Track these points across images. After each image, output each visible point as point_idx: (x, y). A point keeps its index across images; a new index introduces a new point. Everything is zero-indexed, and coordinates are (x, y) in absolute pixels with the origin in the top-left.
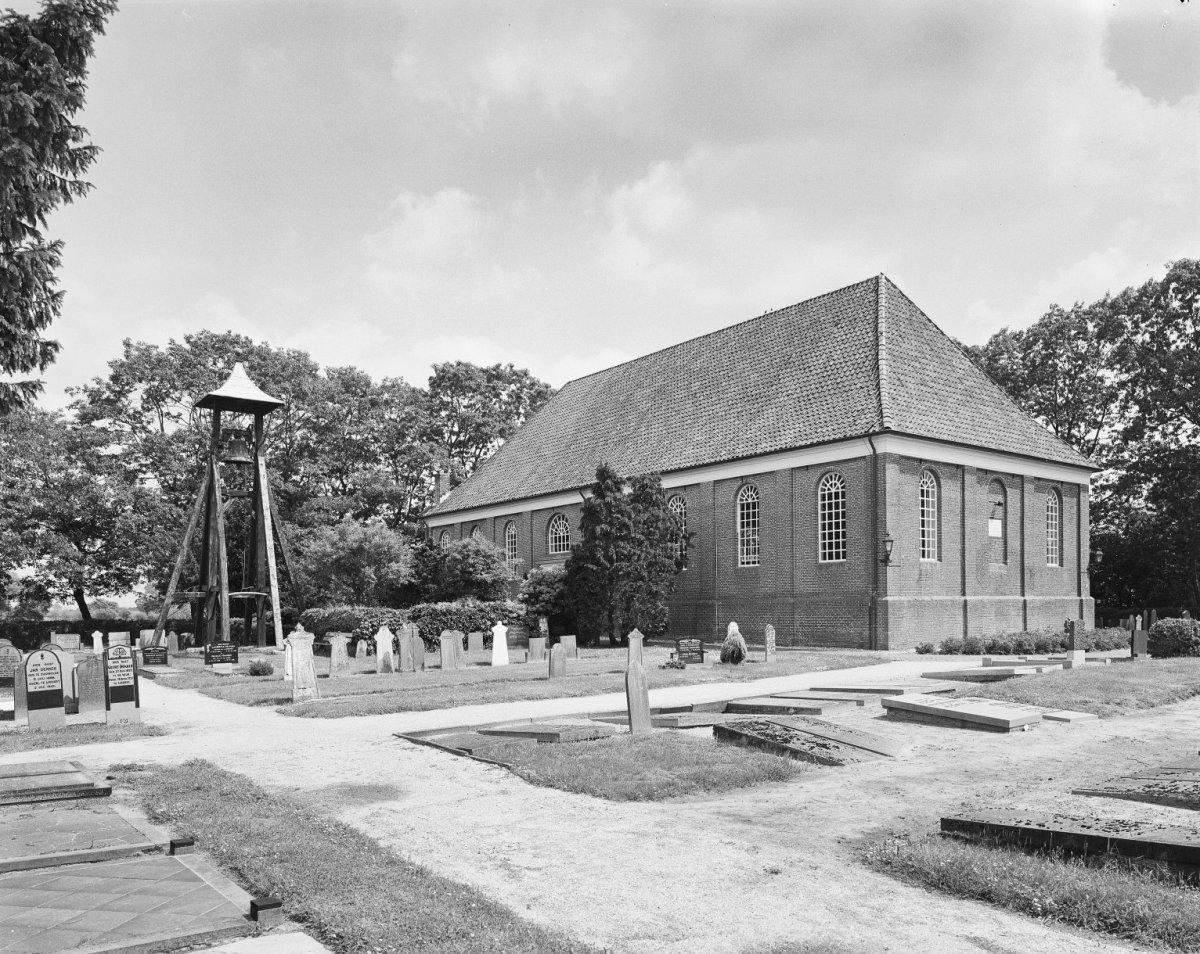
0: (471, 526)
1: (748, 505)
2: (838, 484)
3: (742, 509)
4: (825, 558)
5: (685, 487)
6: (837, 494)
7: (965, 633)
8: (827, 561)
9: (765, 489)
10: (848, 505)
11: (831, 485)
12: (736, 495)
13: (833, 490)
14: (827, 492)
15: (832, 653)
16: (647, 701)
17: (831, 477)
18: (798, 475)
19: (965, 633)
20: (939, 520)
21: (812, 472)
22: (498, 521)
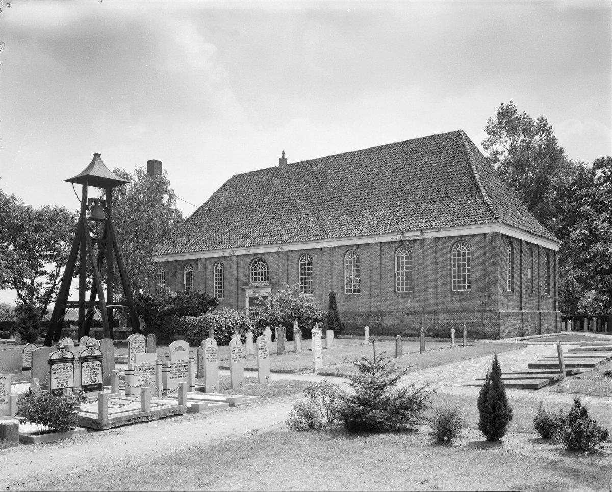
0: (184, 264)
1: (189, 272)
2: (465, 248)
3: (187, 274)
4: (347, 292)
5: (358, 245)
6: (308, 264)
7: (177, 398)
8: (349, 294)
9: (315, 256)
10: (225, 275)
11: (305, 259)
12: (214, 265)
13: (306, 262)
14: (303, 263)
15: (483, 341)
16: (231, 372)
17: (351, 253)
18: (439, 242)
19: (177, 398)
20: (512, 269)
21: (448, 241)
22: (208, 261)
